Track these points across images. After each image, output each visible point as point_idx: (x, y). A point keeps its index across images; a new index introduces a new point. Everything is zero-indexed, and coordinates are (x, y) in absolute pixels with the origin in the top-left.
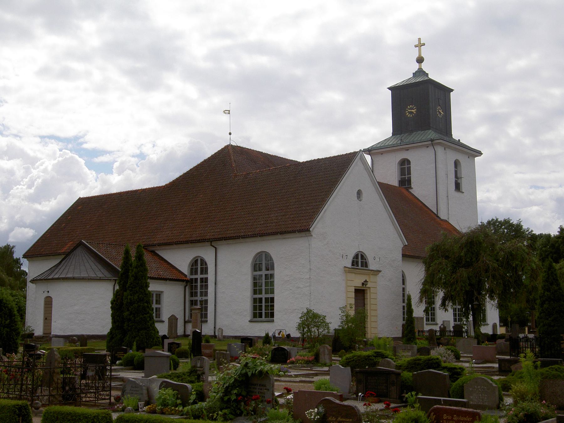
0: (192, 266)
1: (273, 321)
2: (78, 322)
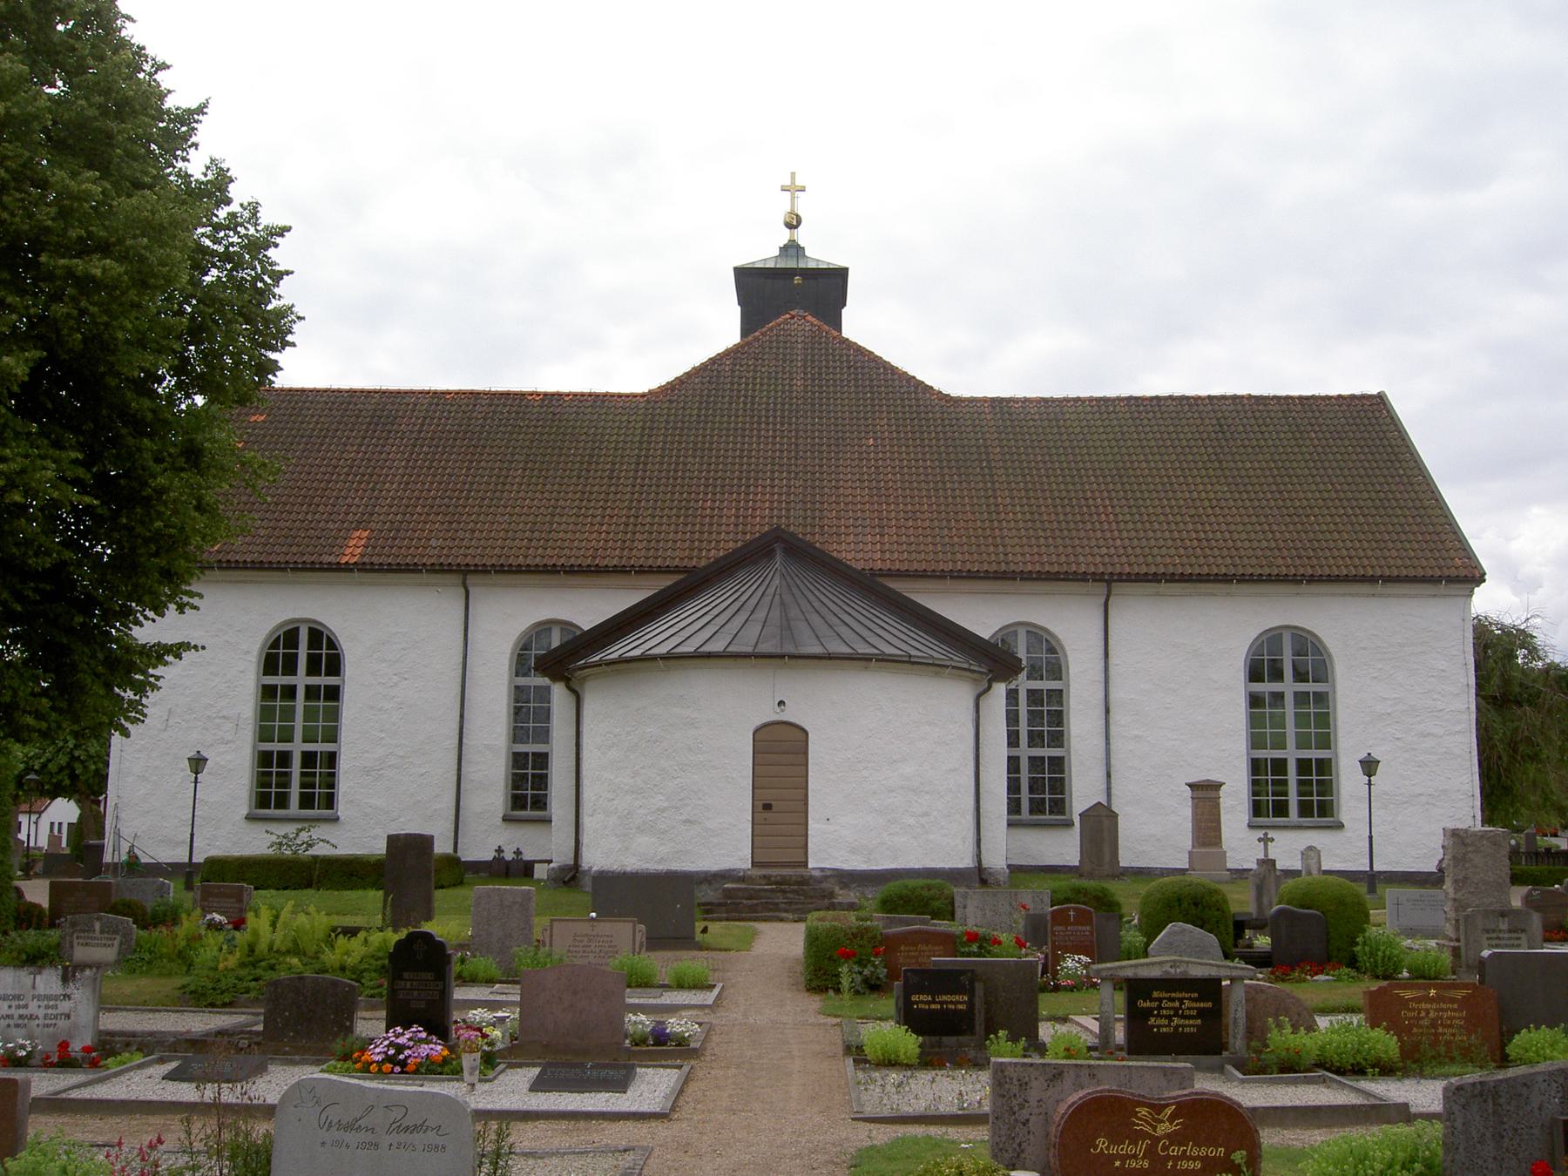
0: (275, 645)
1: (547, 821)
2: (911, 821)
